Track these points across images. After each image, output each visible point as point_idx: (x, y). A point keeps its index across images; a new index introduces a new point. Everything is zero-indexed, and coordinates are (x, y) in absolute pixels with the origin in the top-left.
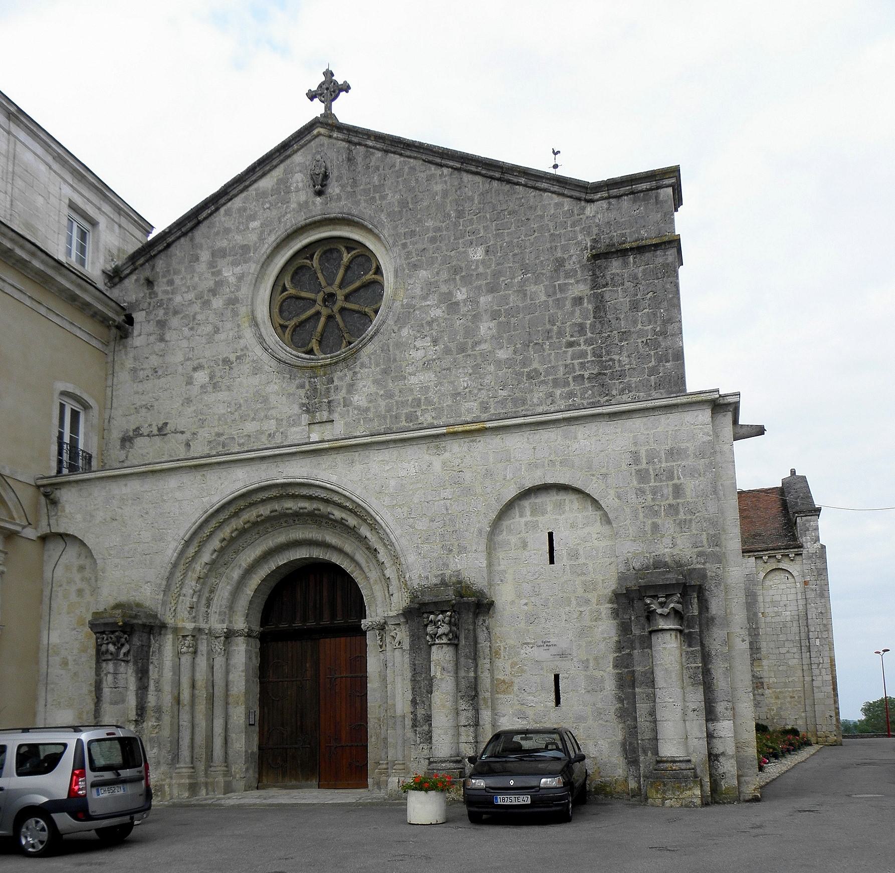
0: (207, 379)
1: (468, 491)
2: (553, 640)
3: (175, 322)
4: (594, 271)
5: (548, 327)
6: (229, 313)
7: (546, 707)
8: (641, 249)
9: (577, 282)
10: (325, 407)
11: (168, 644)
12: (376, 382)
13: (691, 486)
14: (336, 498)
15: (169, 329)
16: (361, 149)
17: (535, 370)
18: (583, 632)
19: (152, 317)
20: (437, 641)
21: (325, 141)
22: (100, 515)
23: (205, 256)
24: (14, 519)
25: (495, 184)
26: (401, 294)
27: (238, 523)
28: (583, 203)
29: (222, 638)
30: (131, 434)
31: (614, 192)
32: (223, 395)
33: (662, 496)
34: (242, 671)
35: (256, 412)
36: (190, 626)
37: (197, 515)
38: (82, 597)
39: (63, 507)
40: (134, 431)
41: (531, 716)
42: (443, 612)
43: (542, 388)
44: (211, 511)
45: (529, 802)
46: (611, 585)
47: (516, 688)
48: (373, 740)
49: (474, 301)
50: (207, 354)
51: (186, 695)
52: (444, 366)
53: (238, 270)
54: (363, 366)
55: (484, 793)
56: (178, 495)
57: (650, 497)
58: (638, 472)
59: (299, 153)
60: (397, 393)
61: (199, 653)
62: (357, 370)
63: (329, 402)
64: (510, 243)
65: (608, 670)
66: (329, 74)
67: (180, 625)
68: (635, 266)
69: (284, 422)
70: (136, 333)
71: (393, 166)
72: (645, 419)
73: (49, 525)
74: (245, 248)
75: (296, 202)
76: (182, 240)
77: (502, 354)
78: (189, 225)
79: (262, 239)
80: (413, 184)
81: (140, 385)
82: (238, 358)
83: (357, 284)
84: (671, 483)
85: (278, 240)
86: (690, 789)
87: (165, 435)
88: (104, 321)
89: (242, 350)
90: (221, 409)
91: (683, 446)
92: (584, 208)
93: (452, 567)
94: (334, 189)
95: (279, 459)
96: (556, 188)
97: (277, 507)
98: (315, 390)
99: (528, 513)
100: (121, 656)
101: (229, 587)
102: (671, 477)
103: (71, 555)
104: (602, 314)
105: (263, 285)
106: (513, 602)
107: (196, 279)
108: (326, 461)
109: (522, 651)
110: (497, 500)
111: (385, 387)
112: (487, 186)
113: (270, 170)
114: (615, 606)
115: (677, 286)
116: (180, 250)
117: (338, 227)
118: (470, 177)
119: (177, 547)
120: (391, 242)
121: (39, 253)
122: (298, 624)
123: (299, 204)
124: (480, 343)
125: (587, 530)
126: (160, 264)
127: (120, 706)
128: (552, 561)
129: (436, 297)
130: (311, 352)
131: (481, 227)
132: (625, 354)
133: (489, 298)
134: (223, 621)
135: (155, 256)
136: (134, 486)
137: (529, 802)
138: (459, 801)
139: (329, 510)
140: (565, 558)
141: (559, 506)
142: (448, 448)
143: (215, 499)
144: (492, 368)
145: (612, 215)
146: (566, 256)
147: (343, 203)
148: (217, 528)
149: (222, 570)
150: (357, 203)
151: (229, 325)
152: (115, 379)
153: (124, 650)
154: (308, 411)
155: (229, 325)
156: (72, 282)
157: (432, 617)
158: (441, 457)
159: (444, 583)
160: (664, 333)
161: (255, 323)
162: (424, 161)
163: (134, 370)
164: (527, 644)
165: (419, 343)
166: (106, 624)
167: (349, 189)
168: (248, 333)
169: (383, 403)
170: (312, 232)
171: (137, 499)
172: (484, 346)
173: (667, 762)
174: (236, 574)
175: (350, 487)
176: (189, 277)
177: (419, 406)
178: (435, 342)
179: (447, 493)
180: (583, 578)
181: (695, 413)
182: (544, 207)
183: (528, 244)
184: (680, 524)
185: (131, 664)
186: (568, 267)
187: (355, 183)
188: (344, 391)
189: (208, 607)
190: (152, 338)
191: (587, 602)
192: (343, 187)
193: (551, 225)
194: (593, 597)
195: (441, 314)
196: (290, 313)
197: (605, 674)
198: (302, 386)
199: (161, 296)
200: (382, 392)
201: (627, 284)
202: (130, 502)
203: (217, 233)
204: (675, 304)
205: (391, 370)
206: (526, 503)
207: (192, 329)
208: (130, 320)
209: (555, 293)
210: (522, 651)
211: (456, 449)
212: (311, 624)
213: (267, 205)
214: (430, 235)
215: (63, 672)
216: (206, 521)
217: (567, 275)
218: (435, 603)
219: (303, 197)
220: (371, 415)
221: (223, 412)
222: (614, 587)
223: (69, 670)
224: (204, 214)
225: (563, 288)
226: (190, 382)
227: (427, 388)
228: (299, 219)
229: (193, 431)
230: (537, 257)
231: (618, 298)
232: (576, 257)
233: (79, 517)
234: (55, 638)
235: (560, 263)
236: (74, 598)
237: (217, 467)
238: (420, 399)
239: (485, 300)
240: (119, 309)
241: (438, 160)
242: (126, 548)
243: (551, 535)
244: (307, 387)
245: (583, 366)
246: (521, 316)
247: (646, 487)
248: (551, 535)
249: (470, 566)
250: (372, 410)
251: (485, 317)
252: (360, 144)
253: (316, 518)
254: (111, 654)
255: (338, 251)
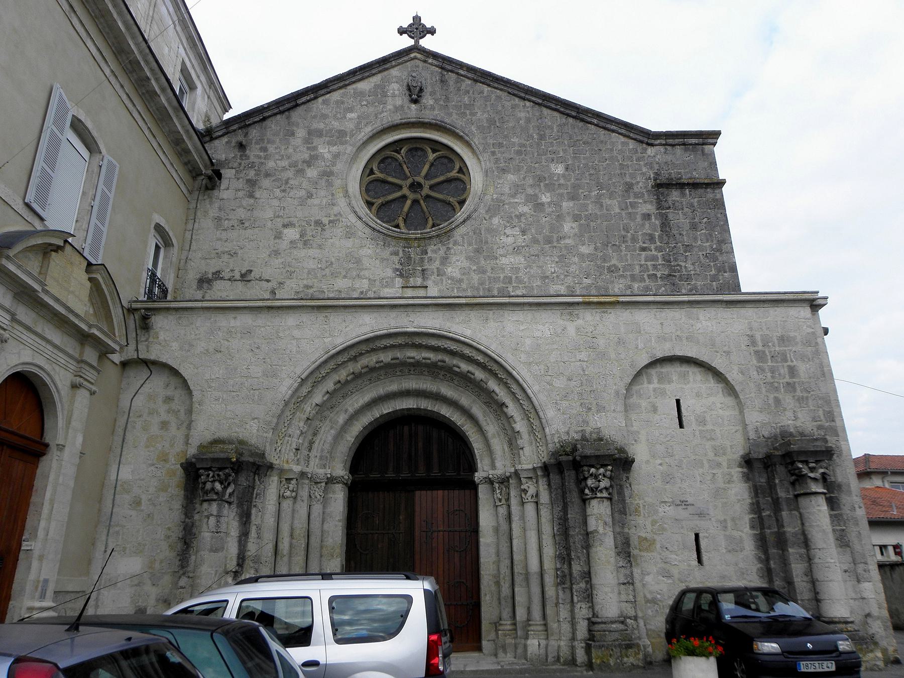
0: (298, 236)
1: (603, 355)
2: (690, 500)
3: (266, 183)
4: (658, 196)
5: (623, 233)
6: (323, 183)
7: (689, 565)
8: (695, 186)
9: (645, 202)
10: (418, 273)
11: (272, 488)
12: (468, 258)
13: (803, 368)
14: (467, 351)
15: (260, 188)
16: (453, 76)
17: (614, 265)
18: (717, 493)
19: (242, 175)
20: (599, 495)
21: (421, 64)
22: (201, 346)
23: (301, 133)
24: (114, 335)
25: (571, 120)
26: (492, 190)
27: (353, 367)
28: (644, 146)
29: (323, 484)
30: (210, 276)
31: (670, 141)
32: (312, 252)
33: (780, 374)
34: (339, 521)
35: (348, 270)
36: (297, 469)
37: (317, 355)
38: (167, 429)
39: (157, 333)
40: (213, 274)
41: (676, 576)
42: (604, 466)
43: (621, 281)
44: (334, 351)
45: (833, 669)
46: (739, 451)
47: (658, 546)
48: (488, 598)
49: (558, 205)
50: (299, 214)
51: (284, 545)
52: (532, 253)
53: (334, 149)
54: (455, 243)
55: (782, 658)
56: (296, 333)
57: (769, 375)
58: (756, 352)
59: (396, 69)
60: (489, 270)
61: (299, 498)
62: (451, 246)
63: (423, 270)
64: (586, 165)
65: (745, 530)
66: (417, 19)
67: (286, 466)
68: (690, 198)
69: (377, 283)
70: (222, 187)
71: (482, 92)
72: (756, 310)
73: (137, 350)
74: (342, 134)
75: (394, 104)
76: (279, 117)
77: (585, 250)
78: (287, 106)
79: (358, 128)
80: (500, 108)
81: (224, 233)
82: (330, 222)
83: (442, 178)
84: (786, 364)
85: (375, 131)
86: (872, 651)
87: (249, 281)
88: (194, 173)
89: (336, 215)
90: (312, 265)
91: (792, 334)
92: (646, 150)
93: (592, 424)
94: (428, 100)
95: (410, 309)
96: (623, 131)
97: (399, 355)
98: (409, 258)
99: (656, 381)
100: (227, 496)
101: (333, 432)
102: (785, 360)
103: (157, 384)
104: (668, 229)
105: (355, 166)
106: (648, 462)
107: (291, 150)
108: (460, 316)
109: (660, 510)
110: (632, 366)
111: (478, 263)
112: (564, 120)
113: (369, 76)
114: (745, 470)
115: (726, 215)
116: (275, 125)
117: (428, 131)
118: (549, 111)
119: (292, 384)
120: (481, 148)
121: (169, 90)
122: (390, 475)
123: (395, 107)
124: (564, 238)
125: (712, 399)
126: (254, 132)
127: (220, 554)
128: (681, 426)
129: (523, 197)
130: (397, 226)
131: (560, 149)
132: (690, 262)
133: (571, 204)
134: (324, 466)
135: (250, 125)
136: (244, 320)
137: (833, 669)
138: (638, 667)
139: (455, 362)
140: (694, 424)
141: (684, 376)
142: (581, 315)
143: (339, 340)
144: (576, 259)
145: (669, 158)
146: (634, 182)
147: (436, 112)
148: (334, 370)
149: (327, 413)
150: (450, 115)
151: (322, 193)
152: (196, 225)
153: (230, 490)
154: (401, 276)
155: (322, 193)
156: (183, 127)
157: (593, 470)
158: (575, 323)
159: (584, 439)
160: (719, 250)
161: (346, 194)
162: (509, 93)
163: (218, 219)
164: (665, 502)
165: (508, 231)
166: (214, 460)
167: (442, 103)
168: (342, 203)
169: (476, 278)
170: (403, 131)
171: (248, 332)
172: (567, 241)
173: (839, 622)
174: (342, 419)
175: (484, 341)
176: (283, 147)
177: (510, 282)
178: (524, 232)
179: (583, 356)
180: (713, 443)
181: (798, 309)
182: (613, 143)
183: (601, 168)
184: (798, 400)
185: (234, 506)
186: (636, 190)
187: (447, 99)
188: (437, 262)
189: (310, 450)
190: (241, 194)
191: (719, 465)
192: (436, 100)
193: (619, 157)
194: (723, 460)
195: (528, 211)
196: (376, 193)
197: (743, 535)
198: (396, 253)
199: (252, 159)
200: (475, 268)
201: (686, 210)
202: (239, 335)
203: (315, 117)
204: (725, 229)
205: (482, 249)
206: (653, 372)
207: (284, 191)
208: (219, 176)
209: (627, 208)
210: (660, 510)
211: (588, 317)
212: (405, 475)
213: (365, 103)
214: (516, 148)
215: (133, 513)
216: (325, 362)
217: (636, 196)
218: (597, 457)
219: (399, 102)
220: (464, 286)
221: (313, 267)
222: (742, 453)
223: (142, 511)
224: (304, 99)
225: (633, 205)
226: (278, 236)
227: (517, 270)
228: (395, 118)
229: (280, 280)
230: (610, 179)
231: (680, 219)
232: (642, 184)
233: (175, 345)
234: (126, 473)
235: (629, 187)
236: (155, 429)
237: (342, 310)
238: (511, 278)
239: (566, 205)
240: (209, 163)
241: (523, 95)
242: (231, 382)
243: (678, 401)
244: (401, 254)
245: (655, 267)
246: (599, 221)
247: (765, 366)
248: (678, 401)
249: (609, 424)
250: (466, 281)
251: (568, 219)
252: (452, 71)
253: (434, 370)
254: (217, 493)
255: (422, 150)
